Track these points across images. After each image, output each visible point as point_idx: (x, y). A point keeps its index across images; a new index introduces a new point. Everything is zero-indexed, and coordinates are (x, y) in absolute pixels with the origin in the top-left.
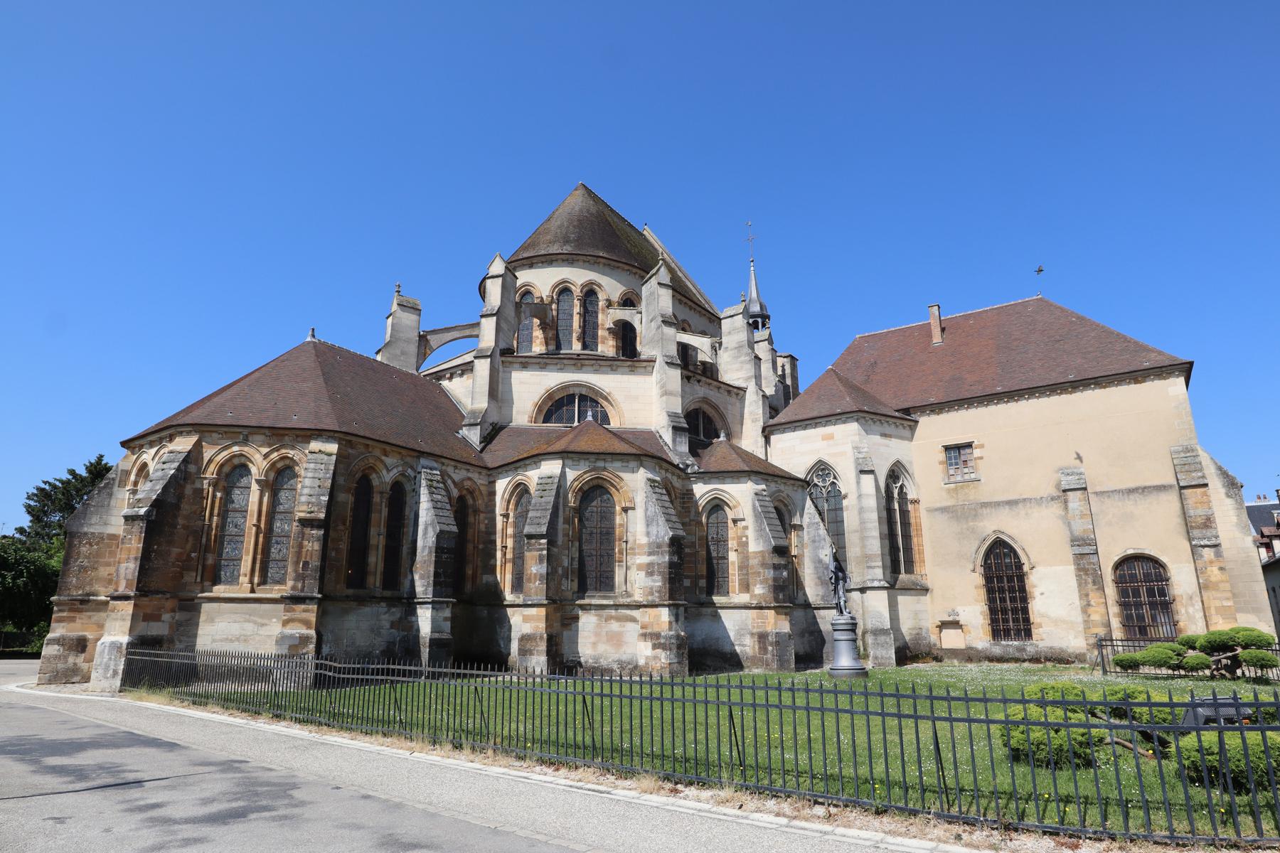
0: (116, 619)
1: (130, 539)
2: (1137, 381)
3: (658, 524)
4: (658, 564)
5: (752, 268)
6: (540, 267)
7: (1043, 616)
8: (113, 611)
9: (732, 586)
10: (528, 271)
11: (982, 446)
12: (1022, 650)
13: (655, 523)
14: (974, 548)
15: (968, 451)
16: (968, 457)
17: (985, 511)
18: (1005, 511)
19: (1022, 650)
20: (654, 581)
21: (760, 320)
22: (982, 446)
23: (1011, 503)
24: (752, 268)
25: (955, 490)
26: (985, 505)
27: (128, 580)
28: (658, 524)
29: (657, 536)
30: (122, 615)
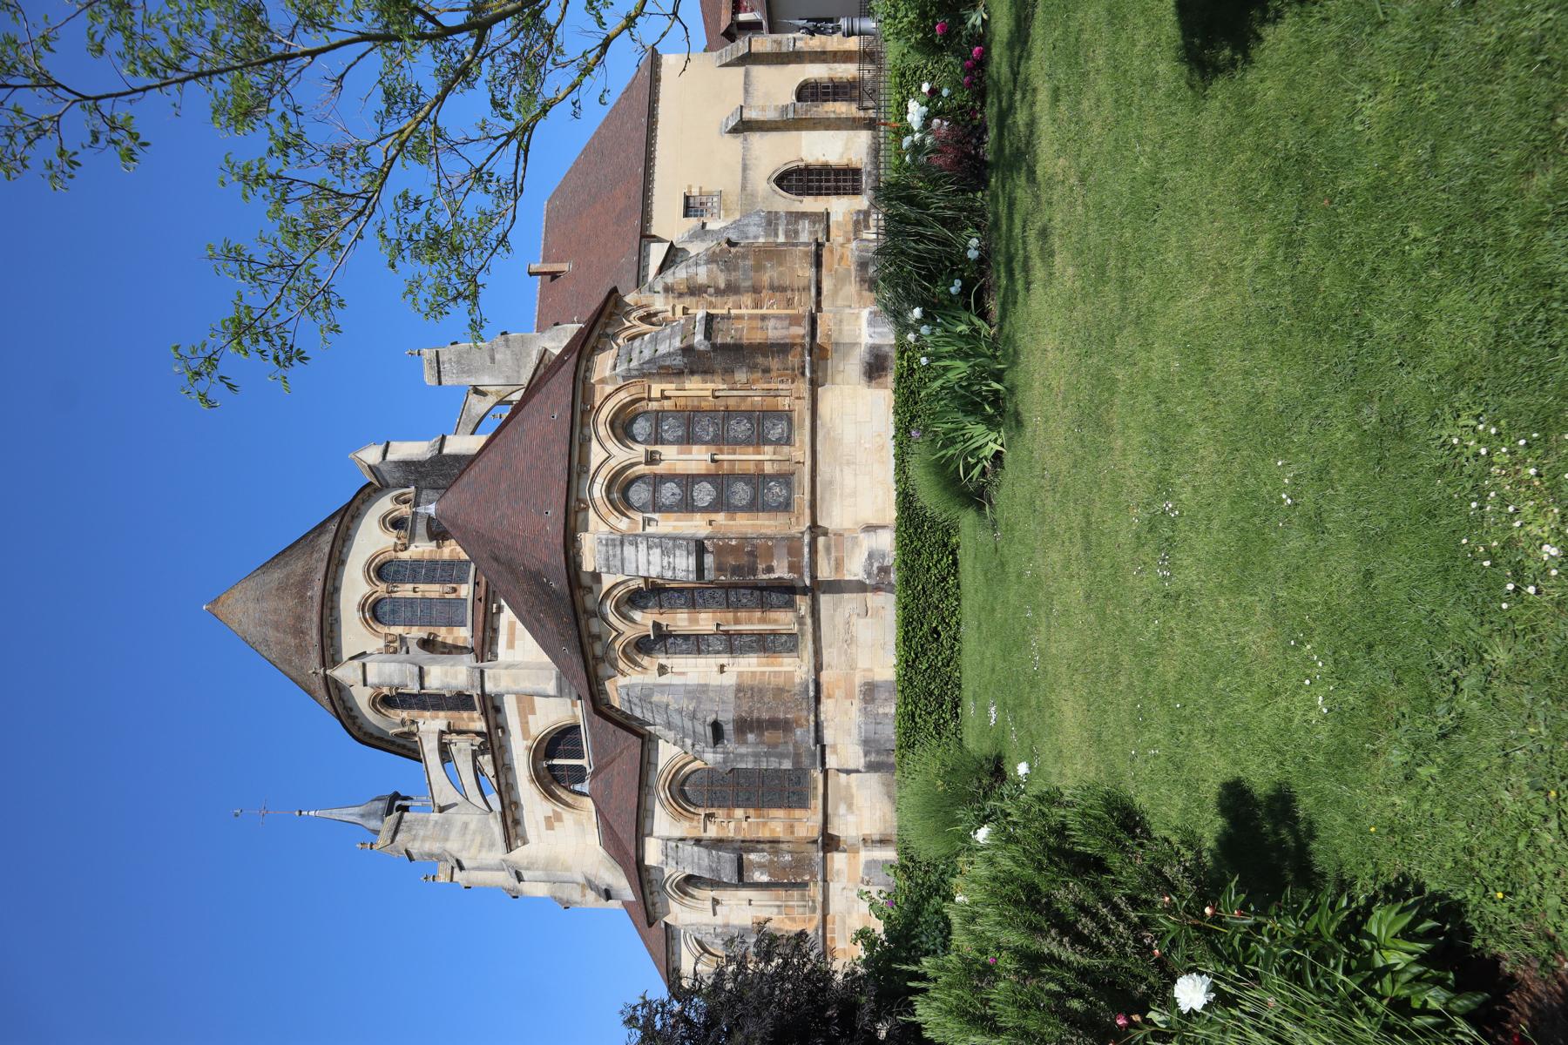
0: (840, 331)
1: (736, 330)
2: (659, 80)
3: (747, 225)
4: (787, 224)
5: (312, 813)
6: (349, 551)
7: (842, 156)
8: (829, 336)
9: (792, 896)
10: (347, 567)
11: (690, 187)
12: (869, 174)
13: (746, 229)
14: (783, 200)
15: (692, 201)
16: (698, 200)
17: (749, 188)
18: (751, 174)
19: (869, 174)
20: (804, 228)
21: (398, 803)
22: (690, 187)
23: (745, 168)
24: (312, 813)
25: (726, 210)
26: (744, 188)
27: (790, 324)
28: (747, 225)
29: (759, 226)
30: (835, 324)
